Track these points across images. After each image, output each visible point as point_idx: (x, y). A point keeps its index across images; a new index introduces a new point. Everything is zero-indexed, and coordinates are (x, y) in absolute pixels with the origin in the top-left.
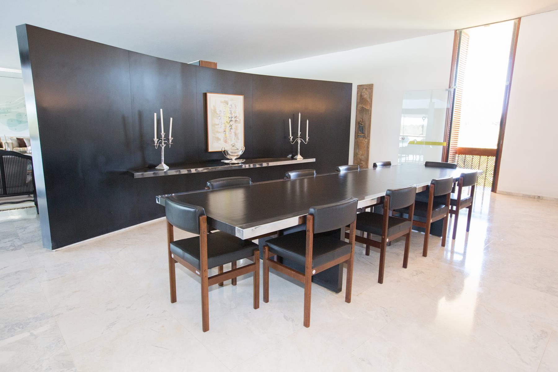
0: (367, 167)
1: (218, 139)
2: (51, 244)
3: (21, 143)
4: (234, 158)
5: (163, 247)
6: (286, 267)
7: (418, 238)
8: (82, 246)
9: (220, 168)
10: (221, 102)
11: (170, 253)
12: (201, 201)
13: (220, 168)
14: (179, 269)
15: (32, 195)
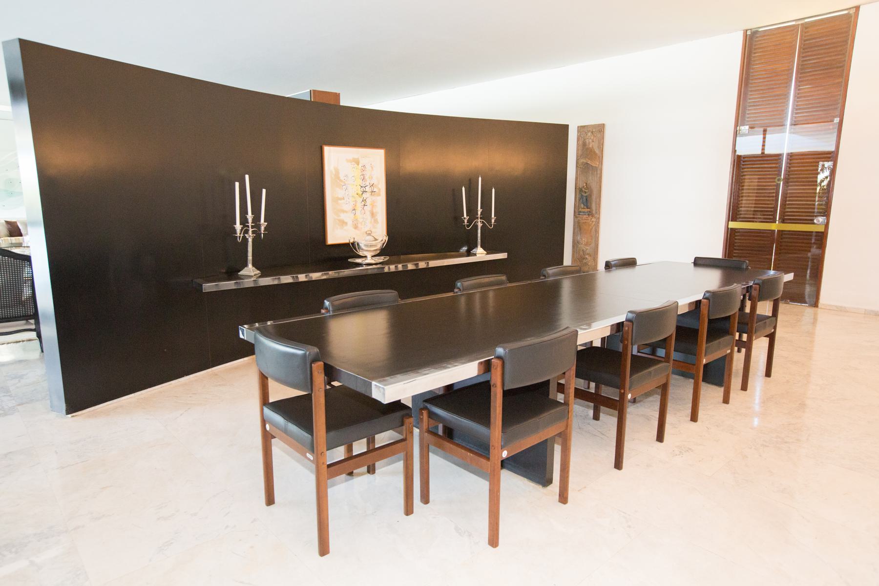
0: (596, 265)
1: (343, 223)
2: (63, 406)
3: (14, 230)
4: (369, 255)
5: (250, 409)
6: (458, 445)
7: (681, 390)
8: (117, 408)
9: (346, 272)
10: (348, 161)
11: (264, 422)
12: (313, 335)
13: (346, 272)
14: (278, 448)
15: (32, 321)
